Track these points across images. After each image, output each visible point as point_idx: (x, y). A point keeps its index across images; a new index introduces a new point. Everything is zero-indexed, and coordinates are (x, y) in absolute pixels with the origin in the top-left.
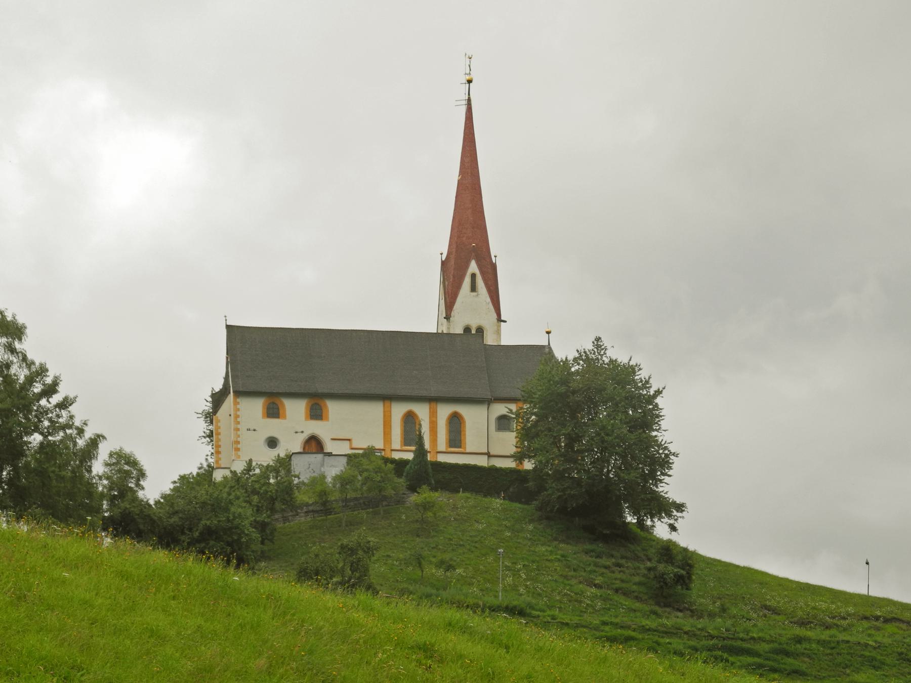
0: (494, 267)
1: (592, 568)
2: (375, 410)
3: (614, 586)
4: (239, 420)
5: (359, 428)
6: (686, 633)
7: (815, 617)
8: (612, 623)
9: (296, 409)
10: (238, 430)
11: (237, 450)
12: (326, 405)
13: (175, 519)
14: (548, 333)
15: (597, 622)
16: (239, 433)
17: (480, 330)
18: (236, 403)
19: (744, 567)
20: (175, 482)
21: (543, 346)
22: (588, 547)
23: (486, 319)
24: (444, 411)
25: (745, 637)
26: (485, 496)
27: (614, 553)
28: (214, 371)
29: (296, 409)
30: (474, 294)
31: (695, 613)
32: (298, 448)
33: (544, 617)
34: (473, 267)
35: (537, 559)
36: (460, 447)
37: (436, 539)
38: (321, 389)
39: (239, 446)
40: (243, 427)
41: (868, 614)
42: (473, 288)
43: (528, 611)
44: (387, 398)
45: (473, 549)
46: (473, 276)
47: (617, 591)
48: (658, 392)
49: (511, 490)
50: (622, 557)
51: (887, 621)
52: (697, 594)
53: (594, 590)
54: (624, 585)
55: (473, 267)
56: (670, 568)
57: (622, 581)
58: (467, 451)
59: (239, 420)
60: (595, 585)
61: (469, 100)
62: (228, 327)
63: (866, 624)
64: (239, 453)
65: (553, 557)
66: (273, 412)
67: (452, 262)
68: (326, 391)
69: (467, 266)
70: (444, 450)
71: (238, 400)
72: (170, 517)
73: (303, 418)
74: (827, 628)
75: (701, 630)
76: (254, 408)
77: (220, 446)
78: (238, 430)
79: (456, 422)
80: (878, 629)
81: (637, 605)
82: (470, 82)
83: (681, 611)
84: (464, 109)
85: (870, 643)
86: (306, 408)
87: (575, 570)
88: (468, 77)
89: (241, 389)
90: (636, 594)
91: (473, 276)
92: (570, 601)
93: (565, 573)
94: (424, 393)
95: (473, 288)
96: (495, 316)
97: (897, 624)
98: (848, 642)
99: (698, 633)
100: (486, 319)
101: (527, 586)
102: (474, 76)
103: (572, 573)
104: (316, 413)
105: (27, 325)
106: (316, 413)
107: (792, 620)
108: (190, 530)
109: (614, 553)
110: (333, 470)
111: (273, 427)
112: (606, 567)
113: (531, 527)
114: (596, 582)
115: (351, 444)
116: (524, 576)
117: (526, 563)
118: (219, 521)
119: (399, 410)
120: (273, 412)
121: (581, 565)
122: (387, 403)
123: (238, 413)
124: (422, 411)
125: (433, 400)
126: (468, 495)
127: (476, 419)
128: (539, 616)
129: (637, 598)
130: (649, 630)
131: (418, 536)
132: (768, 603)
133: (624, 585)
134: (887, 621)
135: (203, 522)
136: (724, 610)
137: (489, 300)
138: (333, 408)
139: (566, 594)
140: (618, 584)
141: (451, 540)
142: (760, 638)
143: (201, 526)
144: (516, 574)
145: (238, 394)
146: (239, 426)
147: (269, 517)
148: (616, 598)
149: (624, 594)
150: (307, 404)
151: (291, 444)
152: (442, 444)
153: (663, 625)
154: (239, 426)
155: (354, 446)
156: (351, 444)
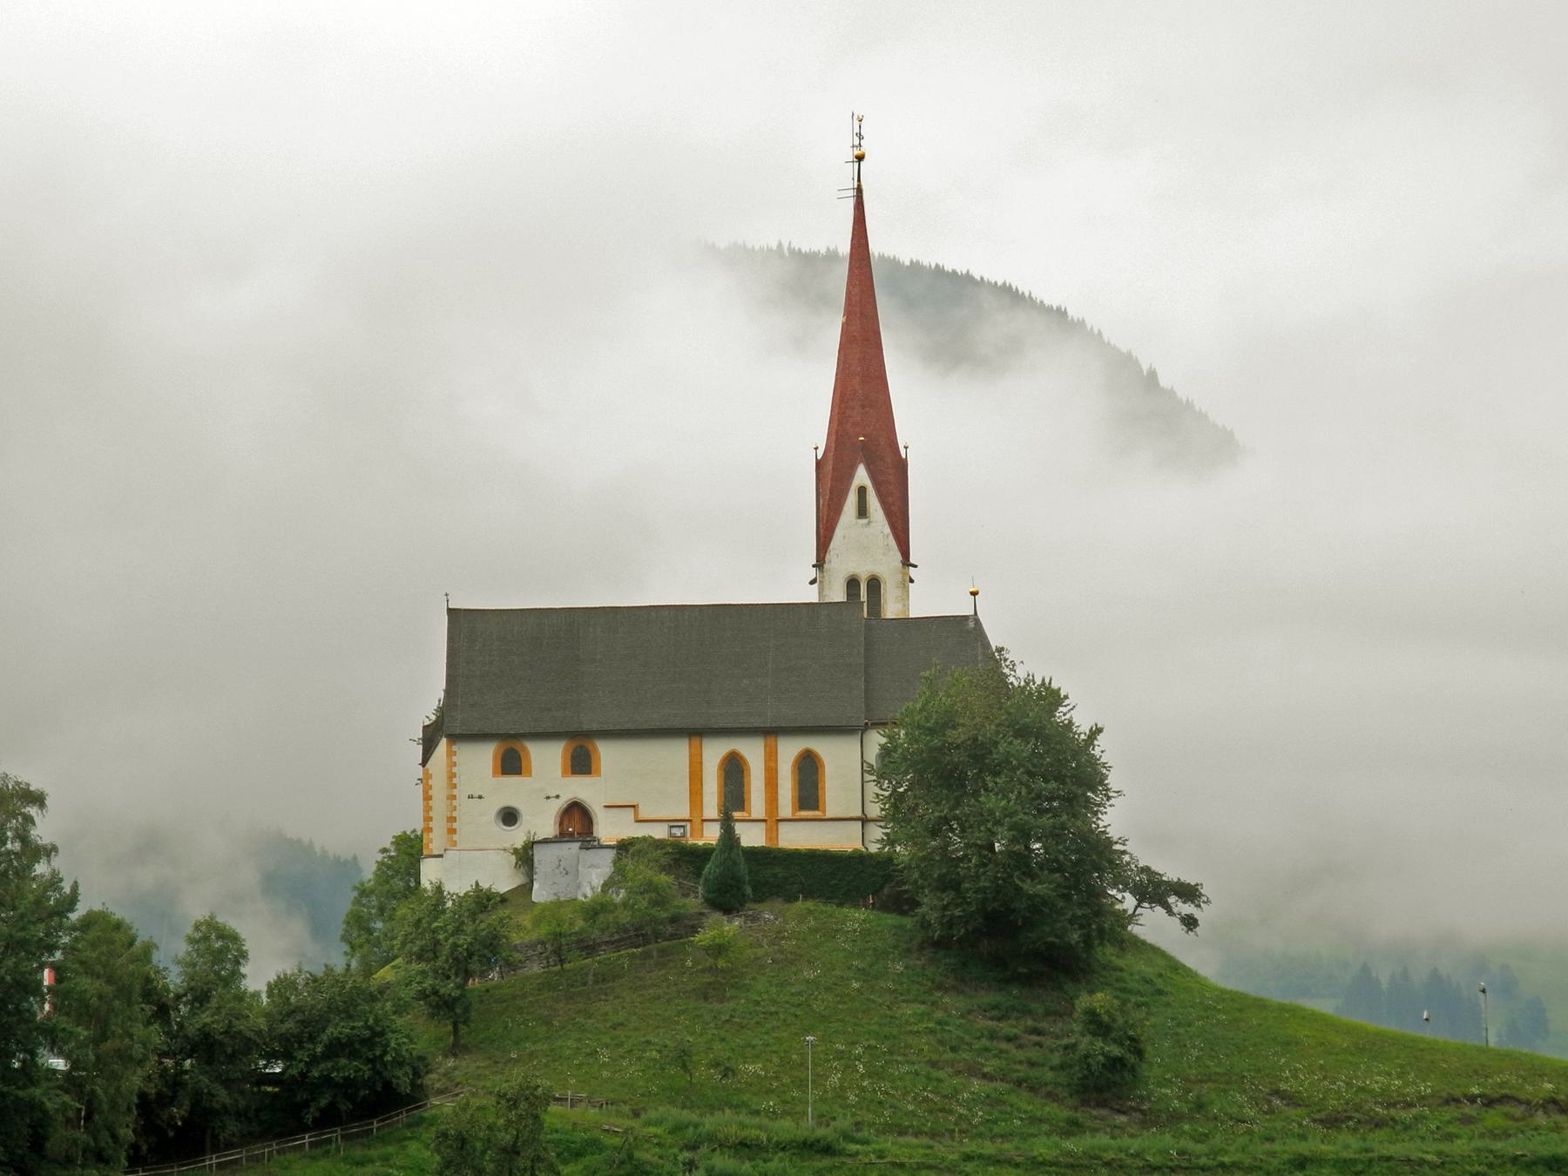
0: (902, 466)
1: (985, 1042)
2: (675, 753)
3: (1015, 1076)
4: (455, 781)
5: (650, 789)
6: (1107, 1164)
7: (1358, 1108)
8: (980, 1156)
9: (546, 757)
10: (454, 797)
11: (452, 831)
12: (596, 749)
13: (290, 1025)
14: (974, 594)
15: (955, 1157)
16: (455, 803)
17: (874, 584)
18: (450, 754)
19: (1282, 1008)
20: (384, 850)
21: (966, 618)
22: (988, 998)
23: (884, 563)
24: (789, 750)
25: (1210, 1163)
26: (841, 905)
27: (1033, 1006)
28: (427, 688)
29: (546, 757)
30: (864, 521)
31: (1150, 1119)
32: (549, 829)
33: (867, 1154)
34: (862, 476)
35: (895, 1032)
36: (816, 808)
37: (732, 1005)
38: (589, 722)
39: (455, 825)
40: (461, 793)
41: (1457, 1093)
42: (862, 512)
43: (843, 1144)
44: (696, 733)
45: (791, 1019)
46: (862, 491)
47: (1019, 1083)
48: (1096, 732)
49: (886, 890)
50: (1048, 1013)
51: (1490, 1102)
52: (1160, 1082)
53: (977, 1085)
54: (1034, 1073)
55: (862, 476)
56: (1099, 1044)
57: (1032, 1064)
58: (828, 815)
59: (455, 781)
60: (984, 1076)
61: (859, 190)
62: (452, 612)
63: (1450, 1112)
64: (455, 837)
65: (921, 1027)
66: (511, 764)
67: (829, 467)
68: (595, 727)
69: (851, 476)
70: (789, 816)
71: (455, 748)
72: (282, 1022)
73: (559, 772)
74: (1377, 1125)
75: (1137, 1155)
76: (479, 759)
77: (431, 819)
78: (454, 797)
79: (809, 768)
80: (1466, 1120)
81: (1052, 1109)
82: (860, 158)
83: (1124, 1113)
84: (851, 203)
85: (1429, 1157)
86: (564, 757)
87: (954, 1049)
88: (857, 152)
89: (458, 731)
90: (1049, 1088)
91: (862, 491)
92: (931, 1112)
93: (935, 1057)
94: (756, 722)
95: (862, 512)
96: (899, 556)
97: (1506, 1108)
98: (1389, 1159)
99: (1129, 1161)
100: (884, 563)
101: (863, 1089)
102: (866, 148)
103: (949, 1055)
104: (581, 764)
105: (47, 790)
106: (581, 764)
107: (1317, 1116)
108: (312, 1039)
109: (1033, 1006)
110: (592, 875)
111: (511, 791)
112: (1009, 1039)
113: (899, 967)
114: (986, 1070)
115: (636, 814)
116: (861, 1069)
117: (873, 1042)
118: (353, 1028)
119: (714, 752)
120: (511, 764)
121: (967, 1038)
122: (696, 741)
123: (455, 770)
124: (752, 751)
125: (771, 732)
126: (810, 904)
127: (845, 763)
128: (857, 1153)
129: (1049, 1095)
130: (1043, 1163)
131: (706, 998)
132: (1283, 1086)
133: (1034, 1073)
134: (1490, 1102)
135: (329, 1030)
136: (1200, 1106)
137: (887, 530)
138: (608, 753)
139: (926, 1099)
140: (1023, 1072)
141: (757, 1003)
142: (1234, 1164)
143: (324, 1037)
144: (849, 1068)
145: (454, 738)
146: (455, 792)
147: (458, 987)
148: (1013, 1098)
149: (1032, 1089)
150: (565, 750)
151: (541, 821)
152: (786, 806)
153: (1069, 1154)
154: (455, 792)
155: (642, 816)
156: (636, 814)
